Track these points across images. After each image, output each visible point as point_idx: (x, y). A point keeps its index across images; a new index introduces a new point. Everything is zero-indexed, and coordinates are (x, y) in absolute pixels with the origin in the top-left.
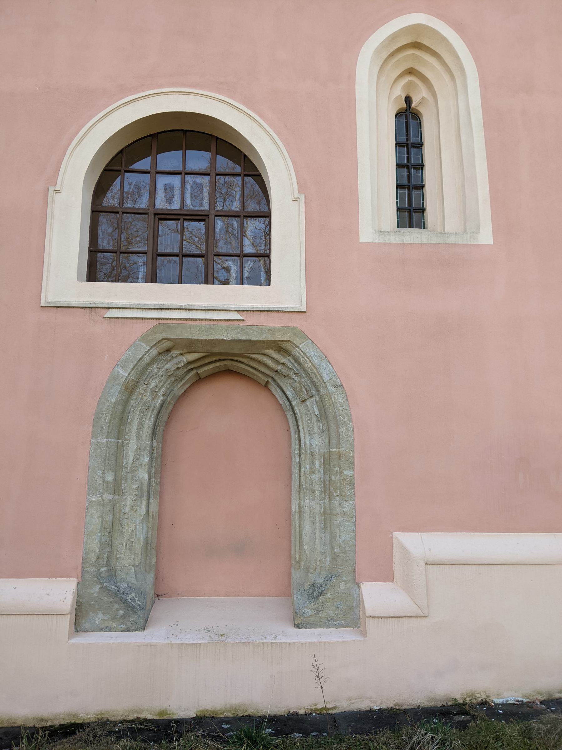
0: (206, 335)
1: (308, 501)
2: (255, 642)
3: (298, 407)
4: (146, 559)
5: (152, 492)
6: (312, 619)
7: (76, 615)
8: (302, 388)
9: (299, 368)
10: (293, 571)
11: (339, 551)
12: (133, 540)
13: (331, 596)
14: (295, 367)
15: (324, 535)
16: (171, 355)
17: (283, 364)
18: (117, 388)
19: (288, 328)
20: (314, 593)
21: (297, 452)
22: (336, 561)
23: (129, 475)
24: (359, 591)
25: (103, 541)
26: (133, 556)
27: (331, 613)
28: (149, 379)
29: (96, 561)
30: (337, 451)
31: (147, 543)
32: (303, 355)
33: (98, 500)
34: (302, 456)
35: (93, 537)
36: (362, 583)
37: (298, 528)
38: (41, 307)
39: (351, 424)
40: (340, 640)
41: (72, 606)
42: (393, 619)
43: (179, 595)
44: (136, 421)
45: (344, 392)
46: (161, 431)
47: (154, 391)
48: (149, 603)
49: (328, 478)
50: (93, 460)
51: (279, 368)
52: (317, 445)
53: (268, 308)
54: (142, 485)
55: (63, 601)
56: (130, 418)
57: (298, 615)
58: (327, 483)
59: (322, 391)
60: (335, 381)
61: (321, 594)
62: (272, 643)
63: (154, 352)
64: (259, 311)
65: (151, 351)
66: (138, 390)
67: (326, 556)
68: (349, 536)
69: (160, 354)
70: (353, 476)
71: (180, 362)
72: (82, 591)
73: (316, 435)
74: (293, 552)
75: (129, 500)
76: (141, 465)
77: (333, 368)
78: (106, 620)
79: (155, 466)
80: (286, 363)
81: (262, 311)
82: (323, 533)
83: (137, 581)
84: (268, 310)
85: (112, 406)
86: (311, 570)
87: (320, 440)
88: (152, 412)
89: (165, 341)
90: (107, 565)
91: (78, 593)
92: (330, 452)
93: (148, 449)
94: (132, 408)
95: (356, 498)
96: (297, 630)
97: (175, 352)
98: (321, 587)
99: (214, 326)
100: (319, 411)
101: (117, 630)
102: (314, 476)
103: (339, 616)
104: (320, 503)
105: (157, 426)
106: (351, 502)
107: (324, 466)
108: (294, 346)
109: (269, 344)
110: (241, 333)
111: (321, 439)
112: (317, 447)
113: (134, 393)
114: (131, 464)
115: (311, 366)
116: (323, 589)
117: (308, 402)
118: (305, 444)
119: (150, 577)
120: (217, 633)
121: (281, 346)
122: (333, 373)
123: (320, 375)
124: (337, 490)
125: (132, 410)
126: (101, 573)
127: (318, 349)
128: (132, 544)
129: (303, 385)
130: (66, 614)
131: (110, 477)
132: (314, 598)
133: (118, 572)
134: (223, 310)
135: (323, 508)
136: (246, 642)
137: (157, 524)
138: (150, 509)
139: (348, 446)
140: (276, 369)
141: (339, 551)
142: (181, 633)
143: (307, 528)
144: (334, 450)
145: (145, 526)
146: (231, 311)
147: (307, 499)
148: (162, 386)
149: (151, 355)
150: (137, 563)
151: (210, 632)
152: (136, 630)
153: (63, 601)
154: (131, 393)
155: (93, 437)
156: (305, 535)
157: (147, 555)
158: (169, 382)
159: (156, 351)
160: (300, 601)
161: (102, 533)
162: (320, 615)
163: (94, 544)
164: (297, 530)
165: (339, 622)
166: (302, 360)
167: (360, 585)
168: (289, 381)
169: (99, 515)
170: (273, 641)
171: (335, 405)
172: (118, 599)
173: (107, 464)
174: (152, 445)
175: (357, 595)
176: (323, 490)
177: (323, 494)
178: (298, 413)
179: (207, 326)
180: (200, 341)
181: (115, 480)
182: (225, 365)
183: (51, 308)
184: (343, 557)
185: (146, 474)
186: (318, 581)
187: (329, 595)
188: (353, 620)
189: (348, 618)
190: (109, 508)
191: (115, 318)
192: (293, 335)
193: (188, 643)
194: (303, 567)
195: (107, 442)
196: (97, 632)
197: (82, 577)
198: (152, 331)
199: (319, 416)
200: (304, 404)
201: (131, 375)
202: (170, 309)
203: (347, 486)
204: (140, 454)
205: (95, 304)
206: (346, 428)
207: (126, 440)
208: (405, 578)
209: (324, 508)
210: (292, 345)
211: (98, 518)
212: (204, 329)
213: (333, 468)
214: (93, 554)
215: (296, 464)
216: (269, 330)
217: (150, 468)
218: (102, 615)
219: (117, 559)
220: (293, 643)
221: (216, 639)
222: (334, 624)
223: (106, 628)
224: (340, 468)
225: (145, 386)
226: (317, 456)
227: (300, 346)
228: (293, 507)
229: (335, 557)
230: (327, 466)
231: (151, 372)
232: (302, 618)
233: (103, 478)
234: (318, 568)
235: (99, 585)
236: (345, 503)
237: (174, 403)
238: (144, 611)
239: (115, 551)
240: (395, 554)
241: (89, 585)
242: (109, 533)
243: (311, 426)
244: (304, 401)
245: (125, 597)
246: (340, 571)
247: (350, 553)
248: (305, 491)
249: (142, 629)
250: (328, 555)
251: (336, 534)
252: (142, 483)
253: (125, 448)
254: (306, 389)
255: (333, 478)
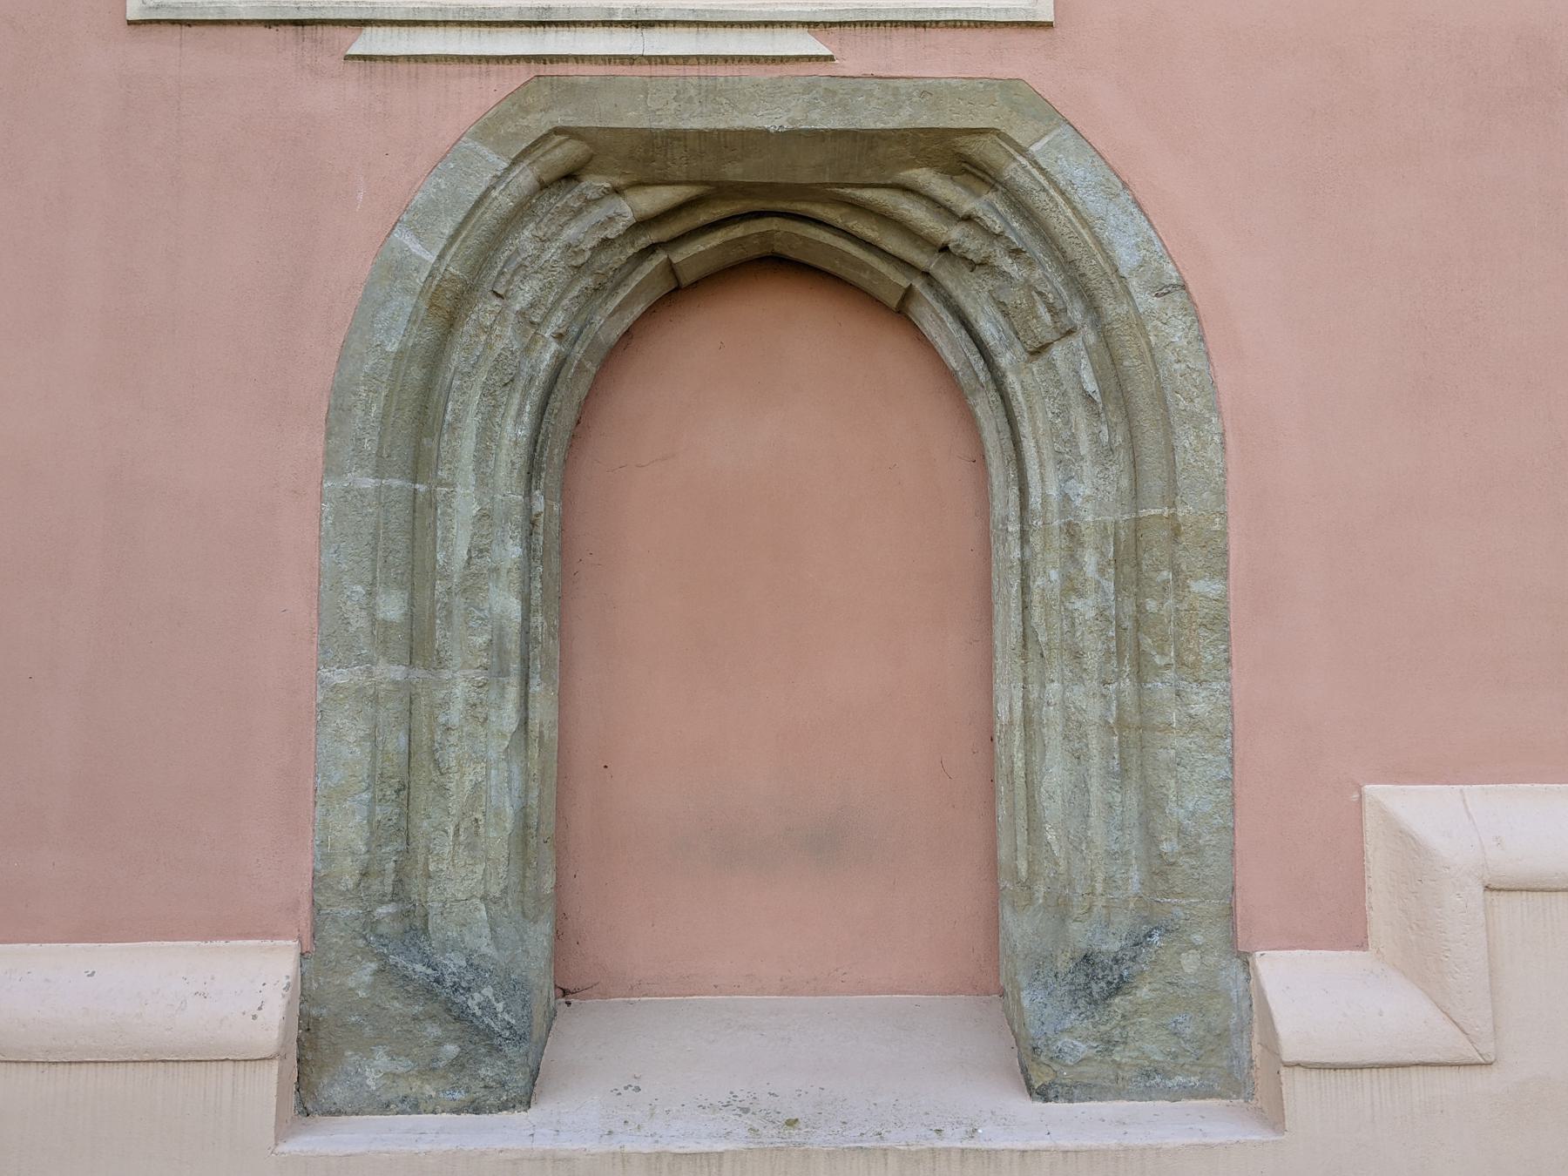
0: (701, 115)
1: (1056, 685)
2: (906, 1148)
3: (1018, 372)
4: (525, 877)
5: (535, 659)
6: (1089, 1070)
7: (298, 1061)
8: (1034, 303)
9: (1025, 232)
10: (1007, 914)
11: (1177, 848)
12: (479, 816)
13: (1153, 995)
14: (1013, 229)
15: (1118, 798)
16: (581, 194)
17: (968, 219)
18: (404, 304)
19: (991, 82)
20: (1093, 985)
21: (1014, 528)
22: (1167, 881)
23: (459, 601)
24: (1248, 980)
25: (379, 818)
26: (480, 869)
27: (1154, 1049)
28: (508, 276)
29: (358, 885)
30: (1165, 515)
31: (526, 826)
32: (1045, 183)
33: (355, 685)
34: (1036, 540)
35: (347, 805)
36: (1258, 954)
37: (1022, 774)
38: (130, 23)
39: (1214, 420)
40: (1195, 1140)
41: (285, 1031)
42: (1374, 1070)
43: (631, 992)
44: (472, 422)
45: (1191, 309)
46: (556, 460)
47: (529, 323)
48: (538, 1019)
49: (1129, 608)
50: (332, 550)
51: (954, 234)
52: (1087, 499)
53: (919, 11)
54: (500, 637)
55: (254, 1017)
56: (453, 410)
57: (1042, 1058)
58: (1128, 624)
59: (1112, 309)
60: (1160, 272)
61: (1119, 987)
62: (963, 1150)
63: (525, 178)
64: (885, 22)
65: (515, 174)
66: (474, 317)
67: (1127, 865)
68: (1212, 797)
69: (543, 186)
70: (1223, 599)
71: (611, 219)
72: (317, 981)
73: (1087, 465)
74: (1003, 853)
75: (460, 686)
76: (496, 570)
77: (1152, 226)
78: (399, 1076)
79: (541, 577)
80: (980, 214)
81: (895, 24)
82: (1117, 788)
83: (498, 950)
84: (918, 17)
85: (390, 366)
86: (1077, 912)
87: (1101, 481)
88: (525, 395)
89: (558, 139)
90: (395, 897)
91: (303, 989)
92: (1137, 520)
93: (518, 517)
94: (456, 377)
95: (1233, 672)
96: (1039, 1104)
97: (594, 183)
98: (1115, 967)
99: (726, 81)
100: (1098, 379)
101: (439, 1109)
102: (1079, 604)
103: (1181, 1060)
104: (1104, 691)
105: (543, 441)
106: (1215, 686)
107: (1116, 568)
108: (1012, 151)
109: (922, 145)
110: (824, 104)
111: (1105, 479)
112: (1089, 506)
113: (462, 326)
114: (463, 564)
115: (1074, 220)
116: (1125, 973)
117: (1057, 352)
118: (1045, 497)
119: (540, 934)
120: (774, 1116)
121: (962, 150)
122: (1150, 241)
123: (1104, 250)
124: (1166, 648)
125: (456, 383)
126: (378, 921)
127: (1097, 158)
128: (478, 827)
129: (1040, 294)
130: (264, 1059)
131: (392, 607)
132: (1096, 1002)
133: (435, 921)
134: (757, 24)
135: (1114, 708)
136: (875, 1149)
137: (555, 765)
138: (531, 715)
139: (1205, 495)
140: (944, 239)
141: (1177, 848)
142: (652, 1115)
143: (1055, 774)
144: (1153, 512)
145: (515, 769)
146: (788, 24)
147: (1053, 681)
148: (553, 304)
149: (513, 189)
150: (495, 891)
151: (749, 1115)
152: (503, 1107)
153: (254, 1017)
154: (451, 323)
155: (327, 472)
156: (1050, 798)
157: (526, 864)
158: (576, 293)
159: (531, 175)
160: (1046, 1011)
161: (373, 792)
162: (1118, 1059)
163: (350, 829)
164: (1020, 782)
165: (1180, 1079)
166: (1039, 200)
167: (1250, 960)
168: (991, 283)
169: (362, 734)
170: (966, 1144)
171: (1158, 355)
172: (436, 1005)
173: (379, 564)
174: (528, 508)
175: (1241, 994)
176: (1114, 649)
177: (1114, 662)
178: (1019, 393)
179: (704, 82)
180: (679, 139)
181: (411, 617)
182: (761, 234)
183: (162, 28)
184: (1192, 867)
185: (516, 601)
186: (1104, 947)
187: (1144, 993)
188: (1230, 1074)
189: (1210, 1066)
190: (393, 709)
191: (384, 58)
192: (1007, 109)
193: (681, 1151)
194: (1041, 901)
195: (378, 489)
196: (370, 1114)
197: (314, 936)
198: (513, 105)
199: (1097, 397)
200: (1041, 362)
201: (448, 258)
202: (574, 23)
203: (1203, 632)
204: (492, 533)
205: (313, 8)
206: (1198, 437)
207: (441, 486)
208: (1413, 938)
209: (1117, 707)
210: (1003, 144)
211: (358, 743)
212: (693, 92)
213: (1153, 574)
214: (349, 859)
215: (1011, 567)
216: (923, 94)
217: (527, 581)
218: (385, 1059)
219: (430, 877)
220: (1035, 1151)
221: (773, 1136)
222: (1165, 1087)
223: (403, 1101)
224: (1176, 572)
225: (496, 301)
226: (1089, 537)
227: (1033, 149)
228: (1002, 708)
229: (1159, 869)
230: (1127, 569)
231: (517, 252)
232: (1056, 1067)
233: (371, 610)
234: (1100, 902)
235: (371, 961)
236: (1195, 690)
237: (594, 370)
238: (525, 1046)
239: (422, 850)
240: (1371, 858)
241: (338, 962)
242: (398, 792)
243: (1065, 434)
244: (1039, 351)
245: (460, 999)
246: (1182, 914)
247: (1215, 855)
248: (1046, 653)
249: (521, 1102)
250: (1134, 861)
251: (1164, 790)
252: (501, 628)
253: (439, 512)
254: (1051, 308)
255: (1151, 605)
